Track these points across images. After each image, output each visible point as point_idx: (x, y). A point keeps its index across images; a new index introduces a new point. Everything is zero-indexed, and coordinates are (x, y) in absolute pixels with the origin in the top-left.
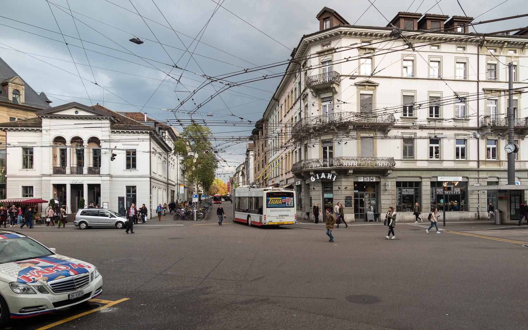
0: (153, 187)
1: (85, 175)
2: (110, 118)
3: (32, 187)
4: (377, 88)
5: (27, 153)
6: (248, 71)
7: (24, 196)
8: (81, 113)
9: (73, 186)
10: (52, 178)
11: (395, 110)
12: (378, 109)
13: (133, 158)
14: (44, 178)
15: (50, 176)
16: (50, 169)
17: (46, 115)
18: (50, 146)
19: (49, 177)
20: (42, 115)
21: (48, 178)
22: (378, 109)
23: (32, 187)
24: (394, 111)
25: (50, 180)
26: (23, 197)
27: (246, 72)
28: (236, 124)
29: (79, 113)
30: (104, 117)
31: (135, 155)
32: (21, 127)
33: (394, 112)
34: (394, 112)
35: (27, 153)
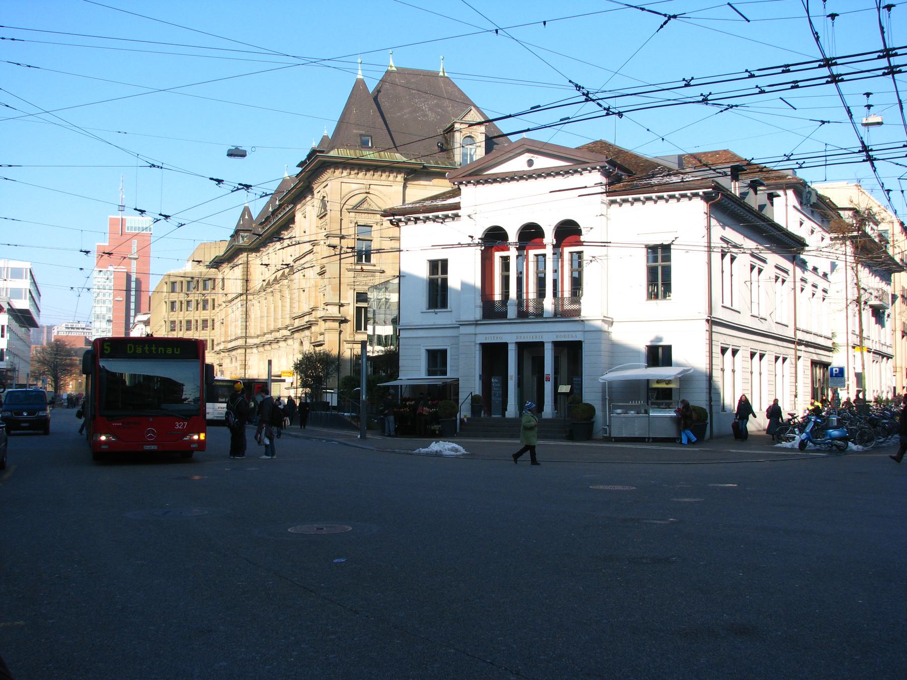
0: (724, 351)
1: (546, 318)
2: (602, 167)
3: (444, 352)
4: (372, 242)
5: (655, 260)
6: (692, 83)
7: (430, 373)
8: (542, 163)
9: (522, 347)
10: (480, 329)
11: (800, 162)
12: (384, 249)
13: (663, 267)
14: (463, 330)
15: (476, 324)
16: (476, 307)
17: (468, 179)
18: (143, 291)
19: (473, 326)
20: (460, 180)
21: (471, 329)
22: (384, 249)
23: (444, 352)
24: (797, 163)
25: (476, 334)
26: (429, 375)
27: (686, 86)
28: (806, 161)
29: (534, 162)
30: (588, 165)
31: (669, 260)
32: (424, 212)
33: (797, 166)
34: (797, 166)
35: (655, 260)
